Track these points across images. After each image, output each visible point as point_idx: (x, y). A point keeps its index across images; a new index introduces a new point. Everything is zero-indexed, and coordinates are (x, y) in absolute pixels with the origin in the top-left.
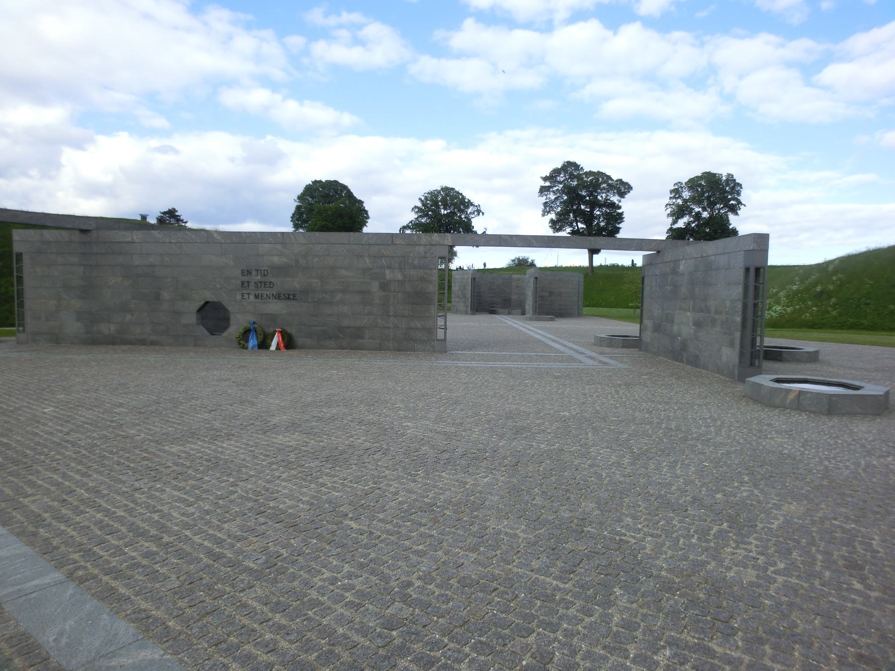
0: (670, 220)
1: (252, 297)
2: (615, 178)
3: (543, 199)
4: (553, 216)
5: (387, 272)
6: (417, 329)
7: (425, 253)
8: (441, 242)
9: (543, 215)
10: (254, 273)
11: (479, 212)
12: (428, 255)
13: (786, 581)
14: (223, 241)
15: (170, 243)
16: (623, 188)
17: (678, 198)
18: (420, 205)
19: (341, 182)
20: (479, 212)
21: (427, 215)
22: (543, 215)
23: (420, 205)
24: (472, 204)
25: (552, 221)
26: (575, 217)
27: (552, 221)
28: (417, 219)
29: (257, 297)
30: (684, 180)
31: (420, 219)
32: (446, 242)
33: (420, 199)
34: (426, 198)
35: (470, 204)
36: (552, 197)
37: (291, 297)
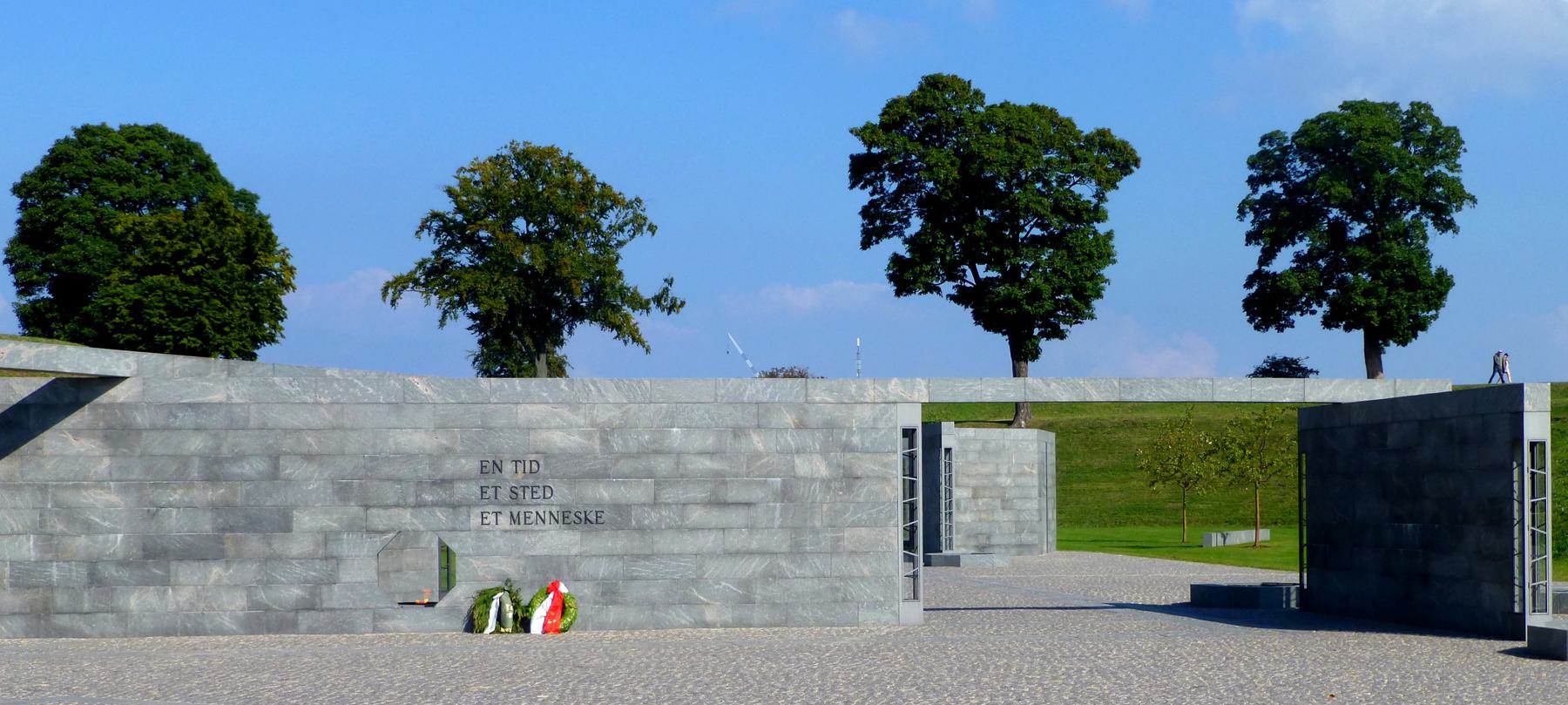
0: (1255, 251)
1: (504, 521)
2: (1086, 127)
3: (863, 196)
4: (894, 246)
5: (798, 461)
6: (863, 578)
7: (875, 420)
8: (906, 396)
9: (866, 244)
10: (508, 467)
11: (639, 224)
12: (881, 424)
13: (1543, 444)
14: (438, 399)
15: (317, 403)
16: (1113, 159)
17: (1276, 178)
18: (446, 206)
19: (173, 127)
20: (639, 224)
21: (471, 240)
22: (866, 244)
23: (446, 206)
24: (616, 201)
25: (896, 260)
26: (946, 237)
27: (896, 260)
28: (437, 253)
29: (514, 519)
30: (1290, 127)
31: (449, 254)
32: (916, 397)
33: (450, 192)
34: (464, 183)
35: (609, 199)
36: (891, 186)
37: (592, 517)
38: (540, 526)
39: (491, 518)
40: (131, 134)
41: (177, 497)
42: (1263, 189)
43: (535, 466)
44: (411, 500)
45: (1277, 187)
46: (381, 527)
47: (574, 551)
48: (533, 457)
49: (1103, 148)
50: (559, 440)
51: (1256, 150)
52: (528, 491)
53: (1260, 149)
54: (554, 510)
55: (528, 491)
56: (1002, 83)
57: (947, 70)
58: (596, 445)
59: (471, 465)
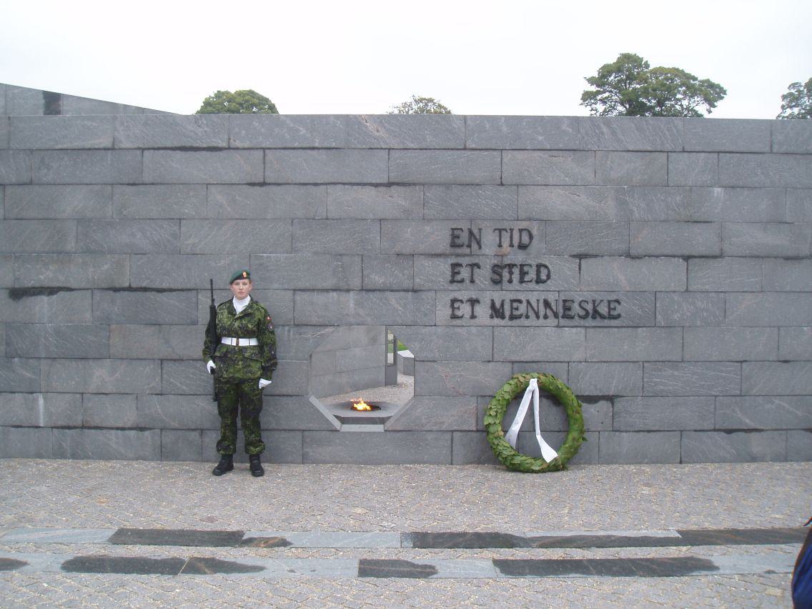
10: (489, 239)
37: (603, 309)
38: (532, 321)
39: (465, 309)
40: (240, 94)
41: (50, 274)
42: (789, 111)
43: (525, 239)
44: (356, 283)
45: (796, 110)
46: (314, 320)
47: (577, 356)
48: (524, 225)
49: (708, 87)
50: (556, 201)
51: (786, 92)
52: (516, 271)
53: (788, 91)
54: (552, 298)
55: (516, 271)
56: (657, 57)
57: (631, 51)
58: (610, 209)
59: (439, 237)
